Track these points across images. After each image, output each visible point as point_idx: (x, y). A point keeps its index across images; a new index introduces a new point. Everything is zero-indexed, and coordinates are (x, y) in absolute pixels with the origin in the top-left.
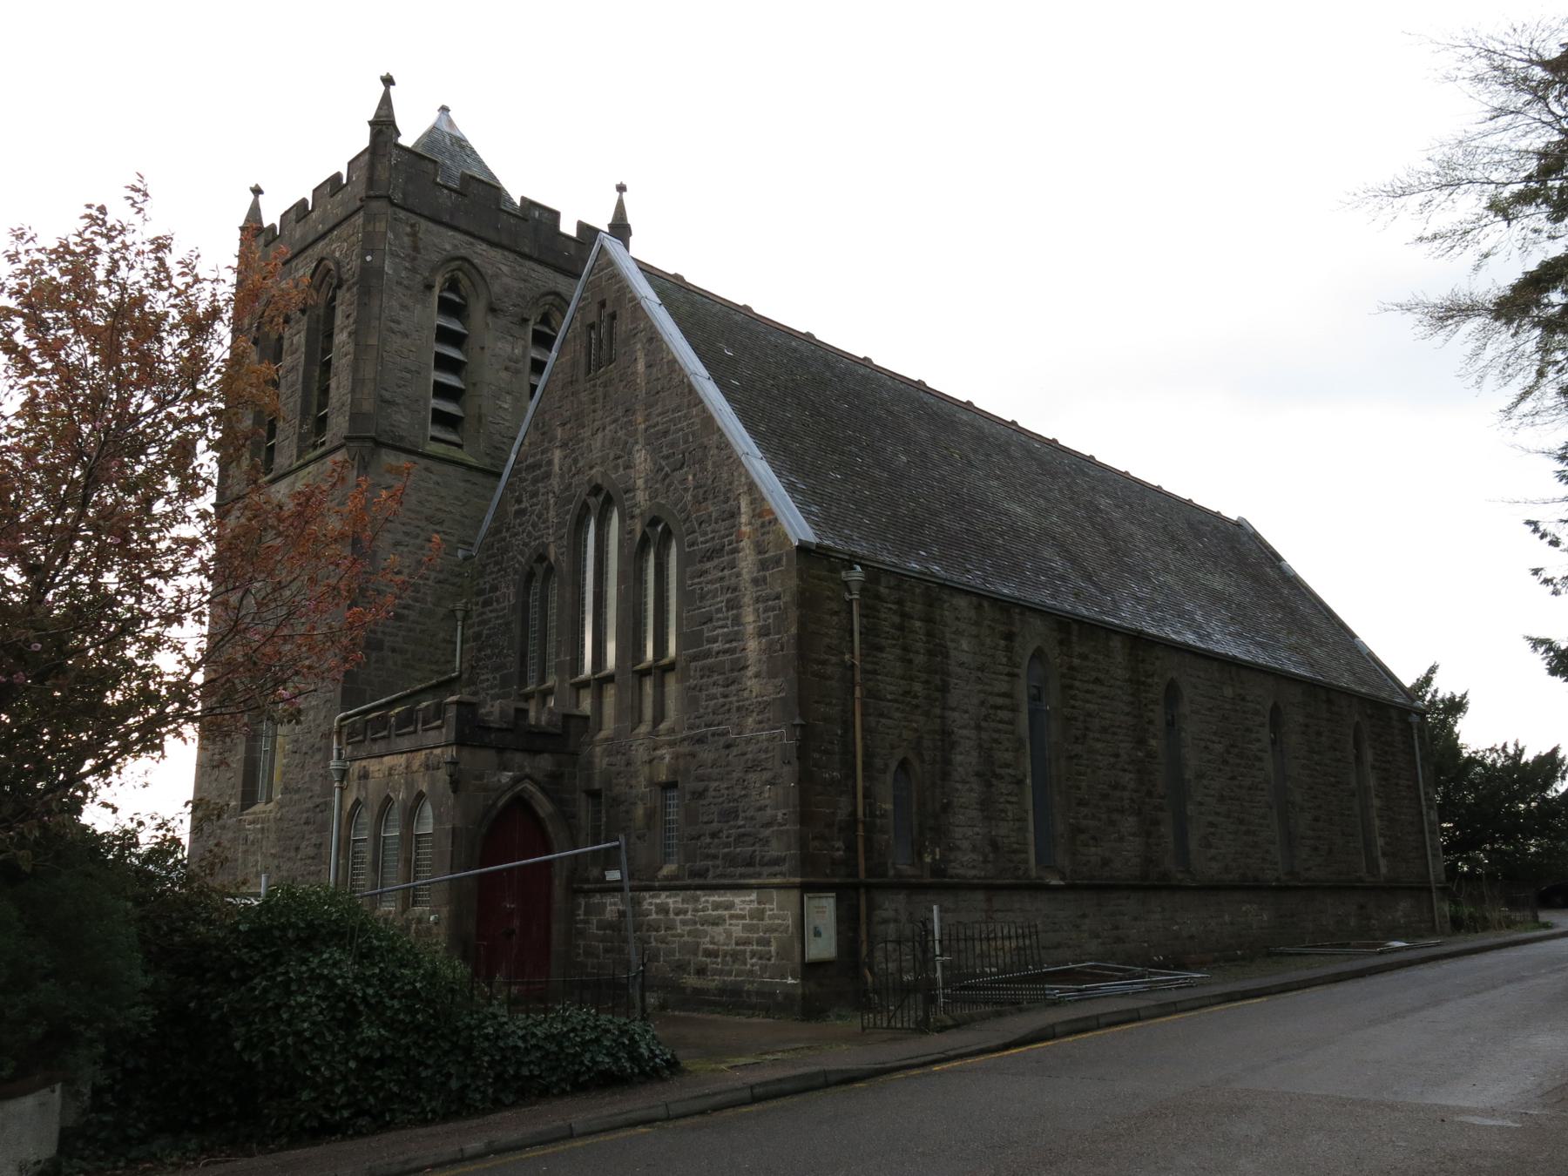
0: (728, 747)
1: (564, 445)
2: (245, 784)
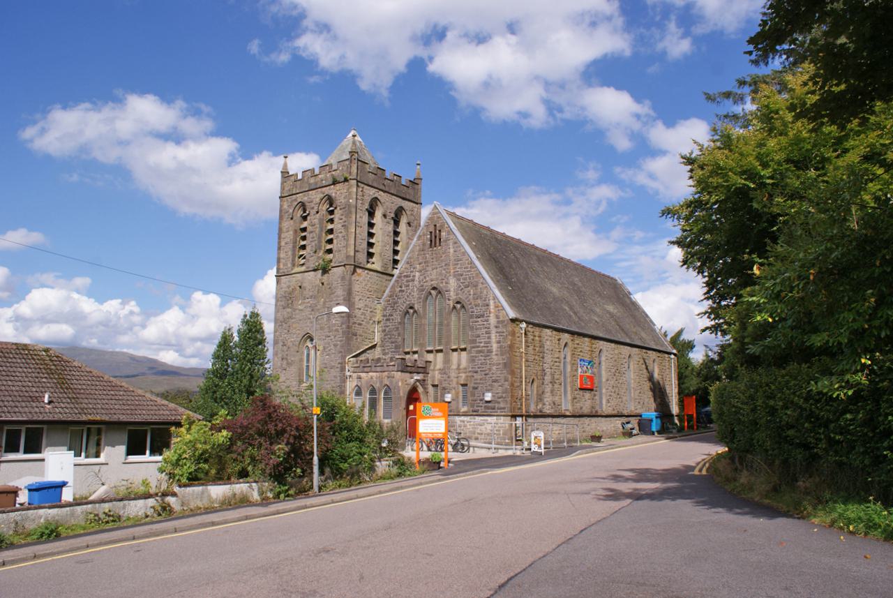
0: (485, 375)
1: (420, 271)
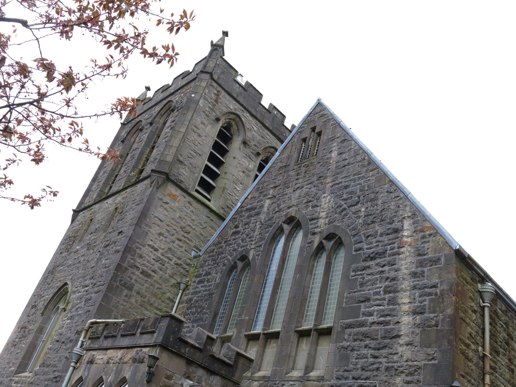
2: (23, 358)
